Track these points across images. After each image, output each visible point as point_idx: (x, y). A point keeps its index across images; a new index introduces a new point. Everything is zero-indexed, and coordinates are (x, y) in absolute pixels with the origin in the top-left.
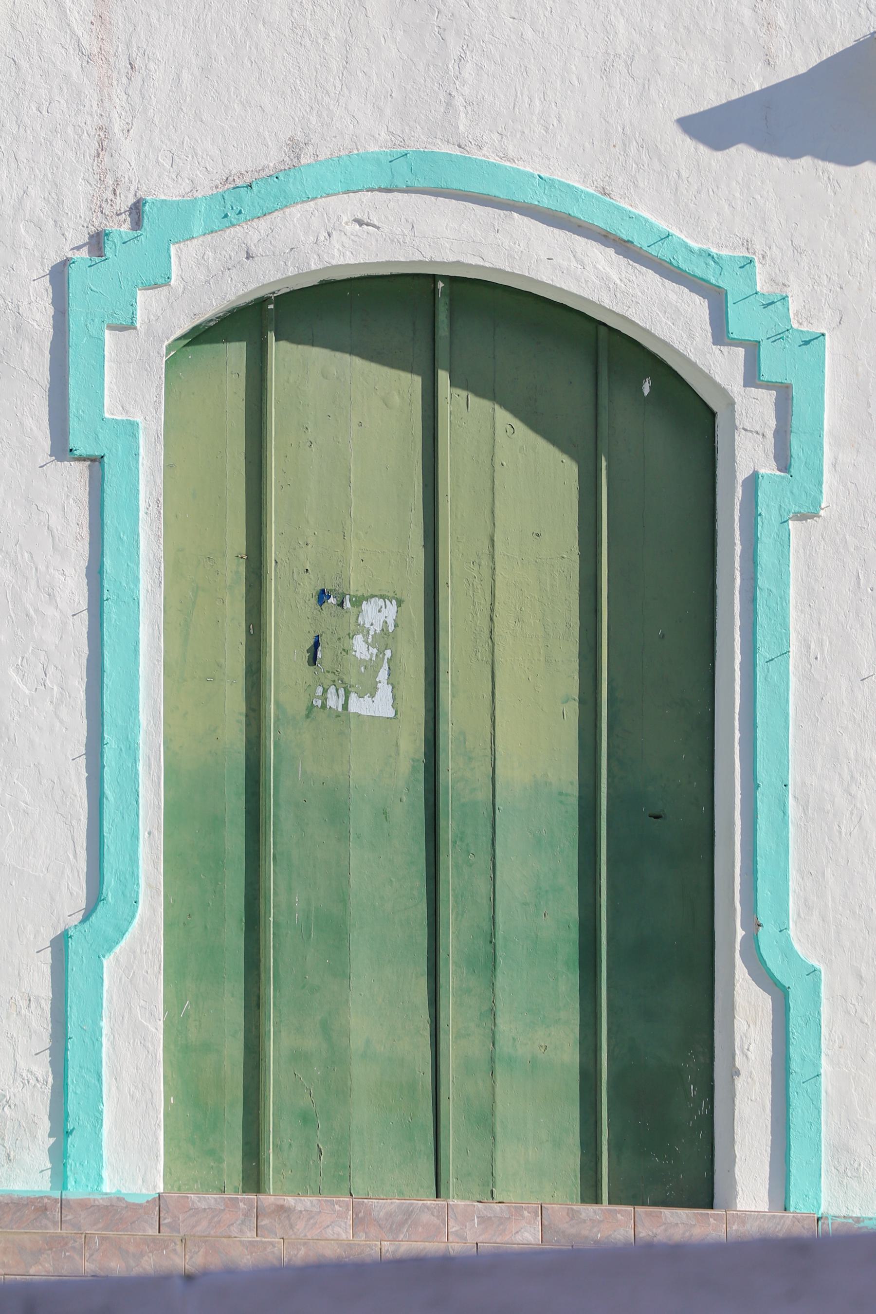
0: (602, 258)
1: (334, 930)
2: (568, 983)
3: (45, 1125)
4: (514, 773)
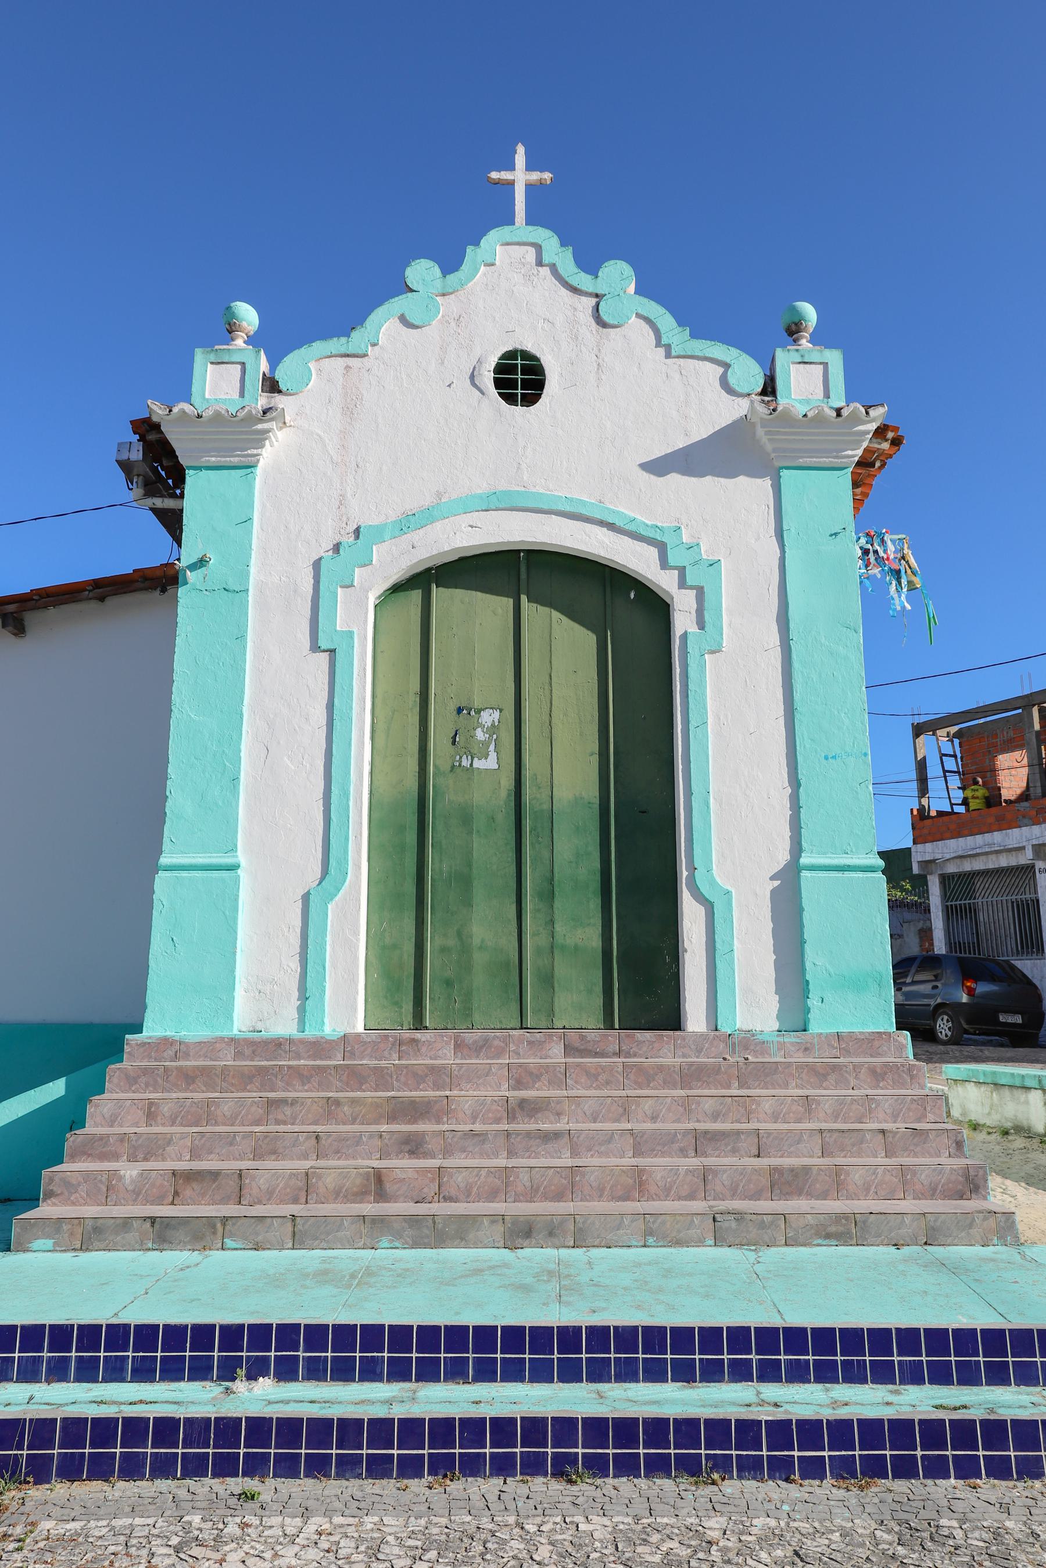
1: (464, 881)
2: (595, 904)
3: (296, 994)
4: (564, 794)
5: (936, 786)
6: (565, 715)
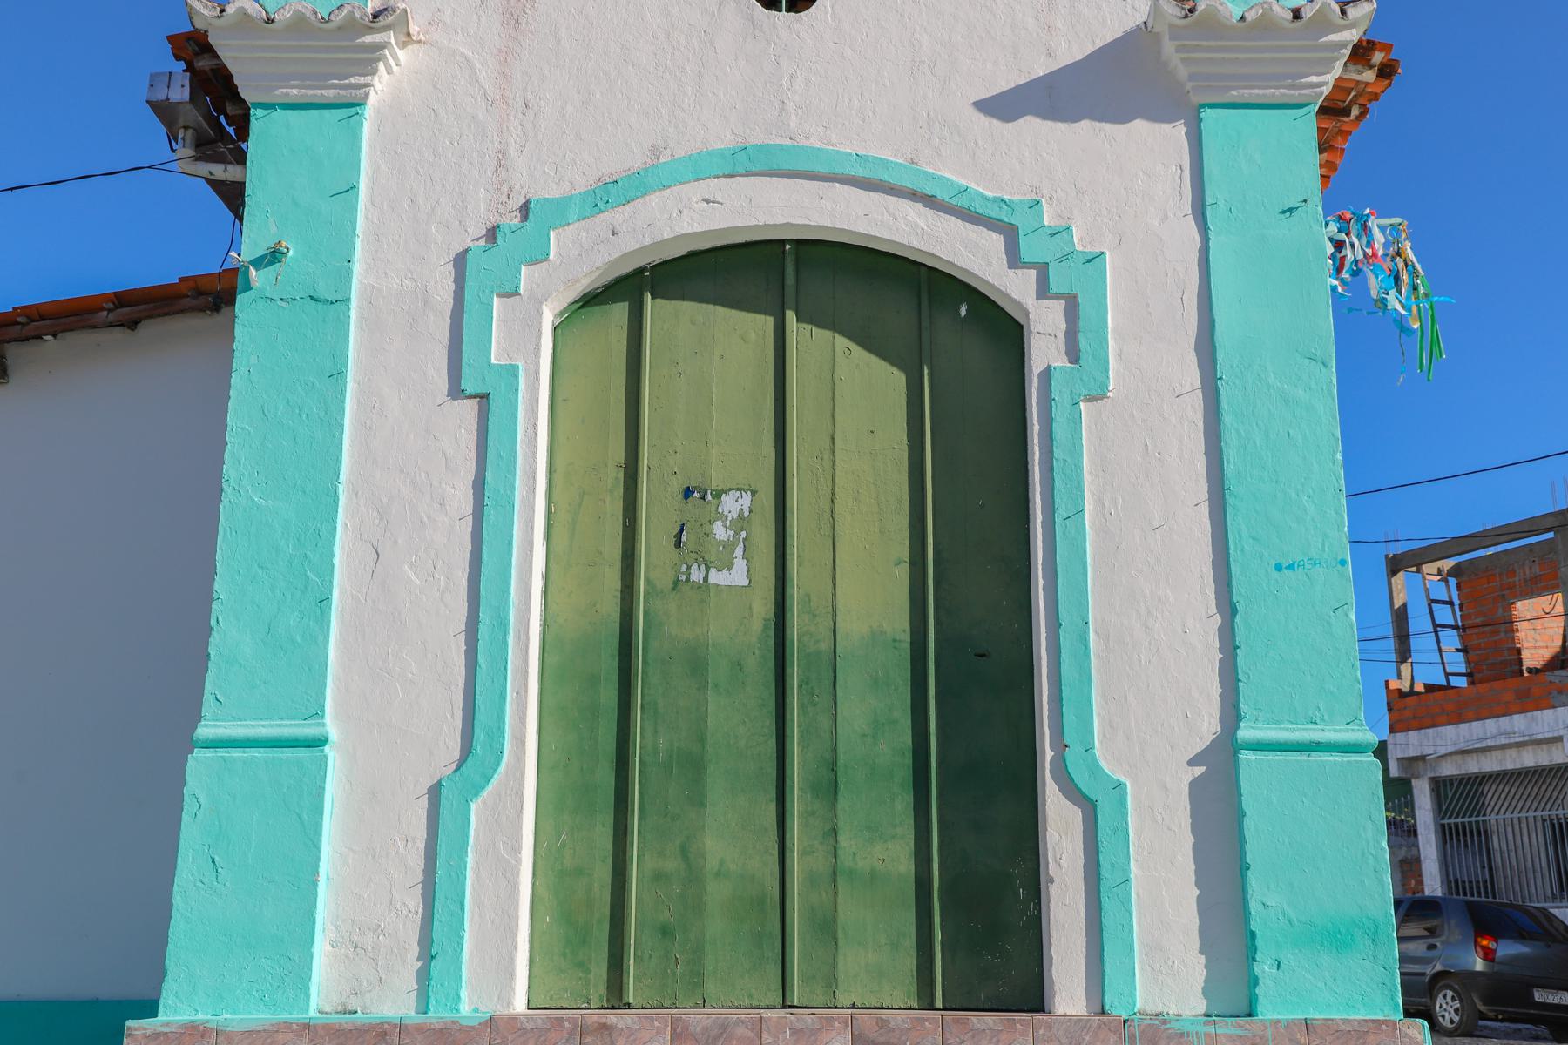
0: (913, 213)
1: (691, 766)
2: (903, 804)
3: (415, 950)
4: (853, 627)
5: (1422, 645)
6: (856, 499)
